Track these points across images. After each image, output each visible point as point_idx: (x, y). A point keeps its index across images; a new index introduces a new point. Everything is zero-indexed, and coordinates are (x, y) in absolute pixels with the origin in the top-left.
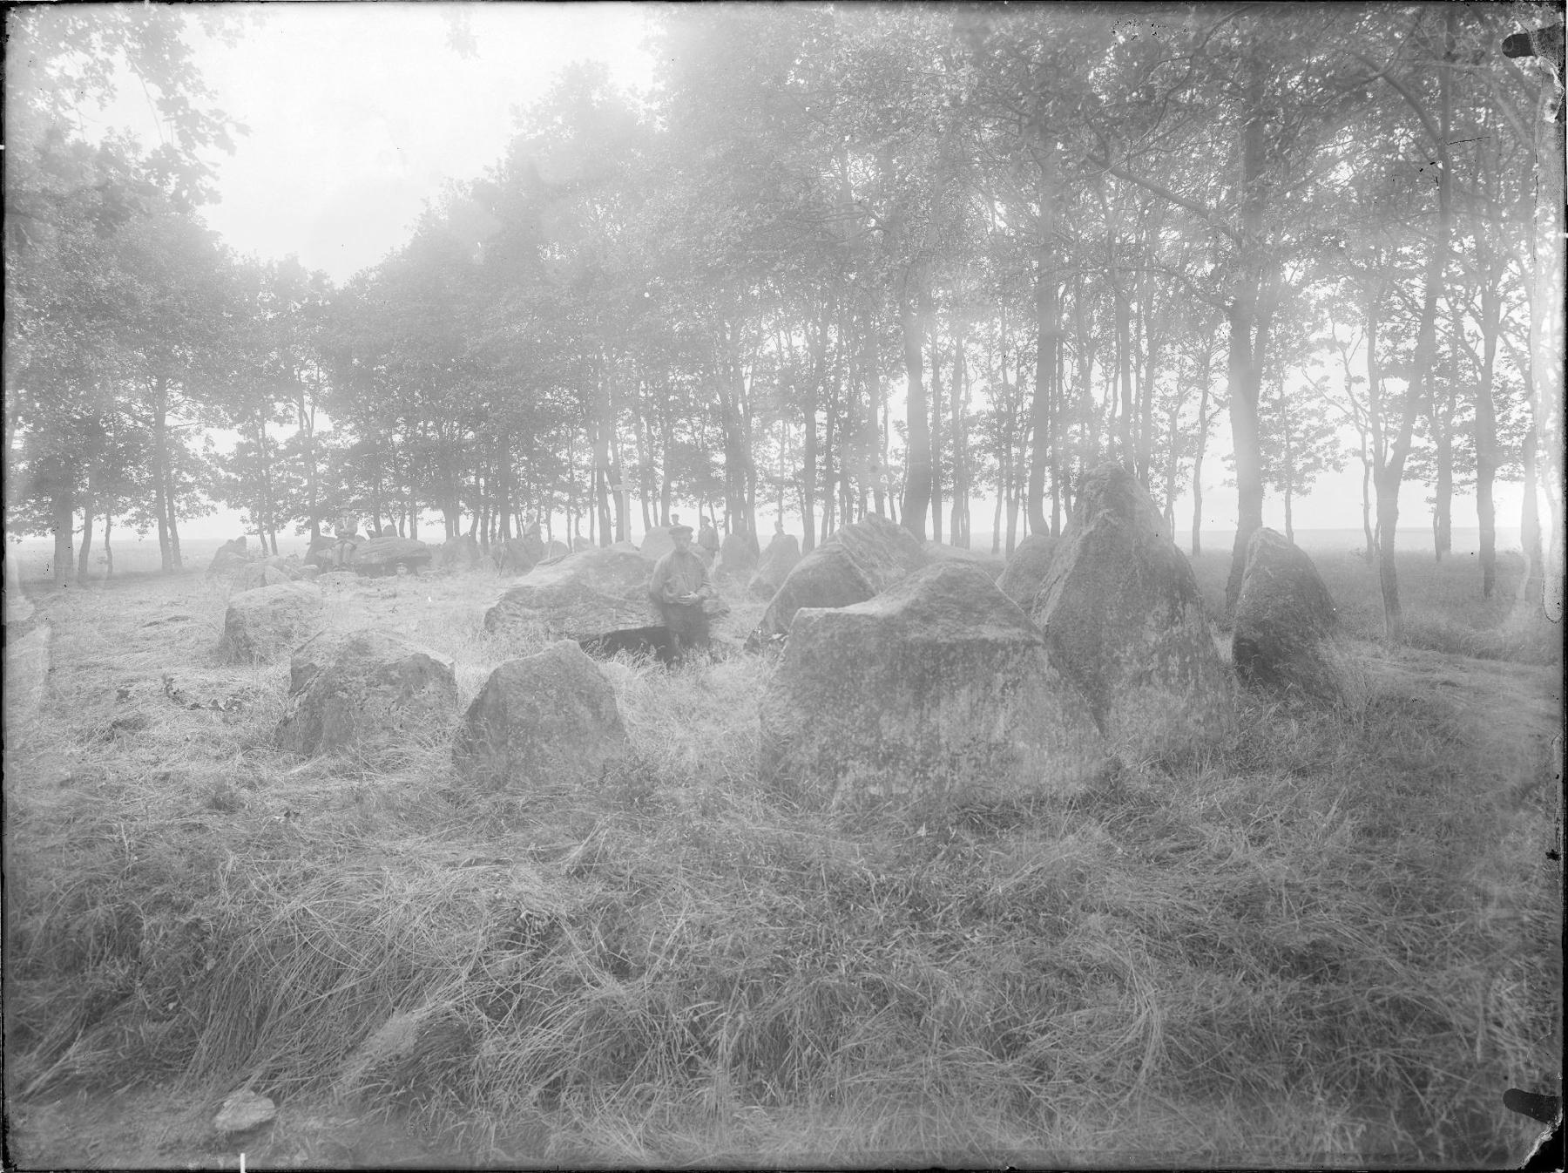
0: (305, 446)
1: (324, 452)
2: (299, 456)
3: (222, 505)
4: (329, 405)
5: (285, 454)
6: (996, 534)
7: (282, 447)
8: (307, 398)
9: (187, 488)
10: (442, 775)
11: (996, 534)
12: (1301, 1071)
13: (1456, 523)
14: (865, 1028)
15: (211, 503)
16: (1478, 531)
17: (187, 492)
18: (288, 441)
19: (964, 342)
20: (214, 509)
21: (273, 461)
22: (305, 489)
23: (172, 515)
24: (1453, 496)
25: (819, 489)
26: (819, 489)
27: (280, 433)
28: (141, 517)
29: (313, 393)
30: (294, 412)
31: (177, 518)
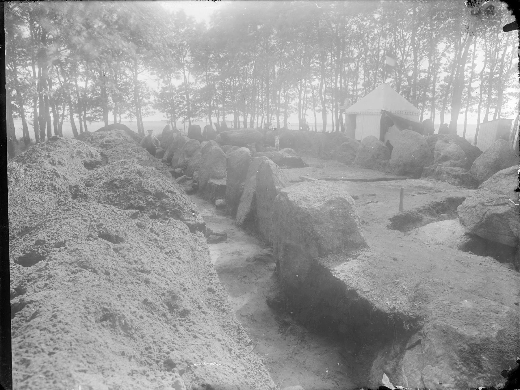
0: (186, 88)
1: (191, 90)
2: (183, 92)
3: (157, 111)
4: (192, 71)
5: (178, 92)
6: (333, 124)
7: (177, 89)
8: (186, 69)
9: (145, 104)
10: (17, 247)
11: (333, 124)
12: (160, 352)
13: (259, 123)
14: (147, 321)
15: (153, 110)
16: (137, 127)
17: (145, 106)
18: (179, 86)
19: (402, 76)
20: (155, 113)
21: (174, 94)
22: (185, 105)
23: (141, 116)
24: (445, 115)
25: (277, 108)
26: (277, 108)
27: (176, 83)
28: (130, 115)
29: (187, 67)
30: (182, 74)
31: (142, 117)
